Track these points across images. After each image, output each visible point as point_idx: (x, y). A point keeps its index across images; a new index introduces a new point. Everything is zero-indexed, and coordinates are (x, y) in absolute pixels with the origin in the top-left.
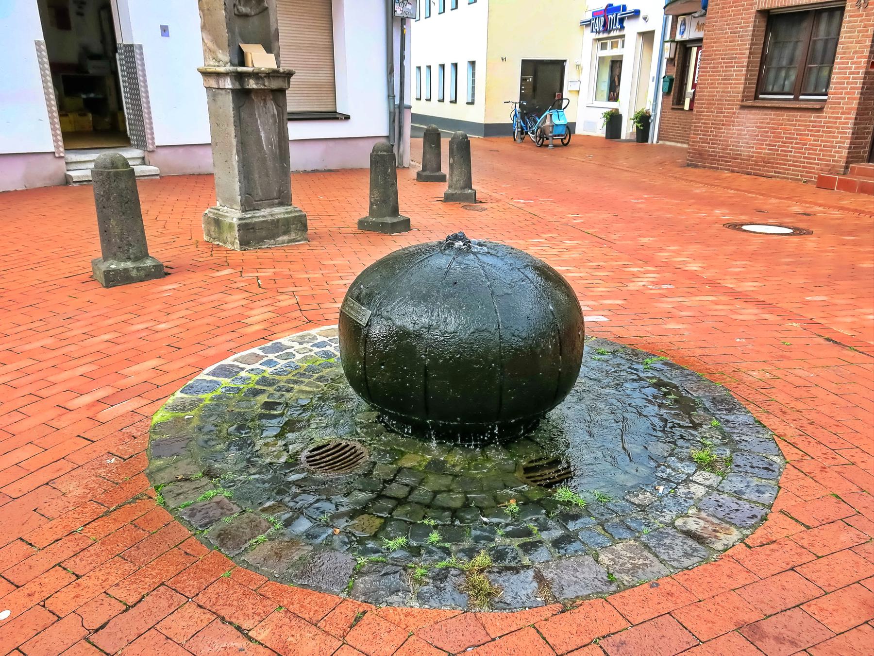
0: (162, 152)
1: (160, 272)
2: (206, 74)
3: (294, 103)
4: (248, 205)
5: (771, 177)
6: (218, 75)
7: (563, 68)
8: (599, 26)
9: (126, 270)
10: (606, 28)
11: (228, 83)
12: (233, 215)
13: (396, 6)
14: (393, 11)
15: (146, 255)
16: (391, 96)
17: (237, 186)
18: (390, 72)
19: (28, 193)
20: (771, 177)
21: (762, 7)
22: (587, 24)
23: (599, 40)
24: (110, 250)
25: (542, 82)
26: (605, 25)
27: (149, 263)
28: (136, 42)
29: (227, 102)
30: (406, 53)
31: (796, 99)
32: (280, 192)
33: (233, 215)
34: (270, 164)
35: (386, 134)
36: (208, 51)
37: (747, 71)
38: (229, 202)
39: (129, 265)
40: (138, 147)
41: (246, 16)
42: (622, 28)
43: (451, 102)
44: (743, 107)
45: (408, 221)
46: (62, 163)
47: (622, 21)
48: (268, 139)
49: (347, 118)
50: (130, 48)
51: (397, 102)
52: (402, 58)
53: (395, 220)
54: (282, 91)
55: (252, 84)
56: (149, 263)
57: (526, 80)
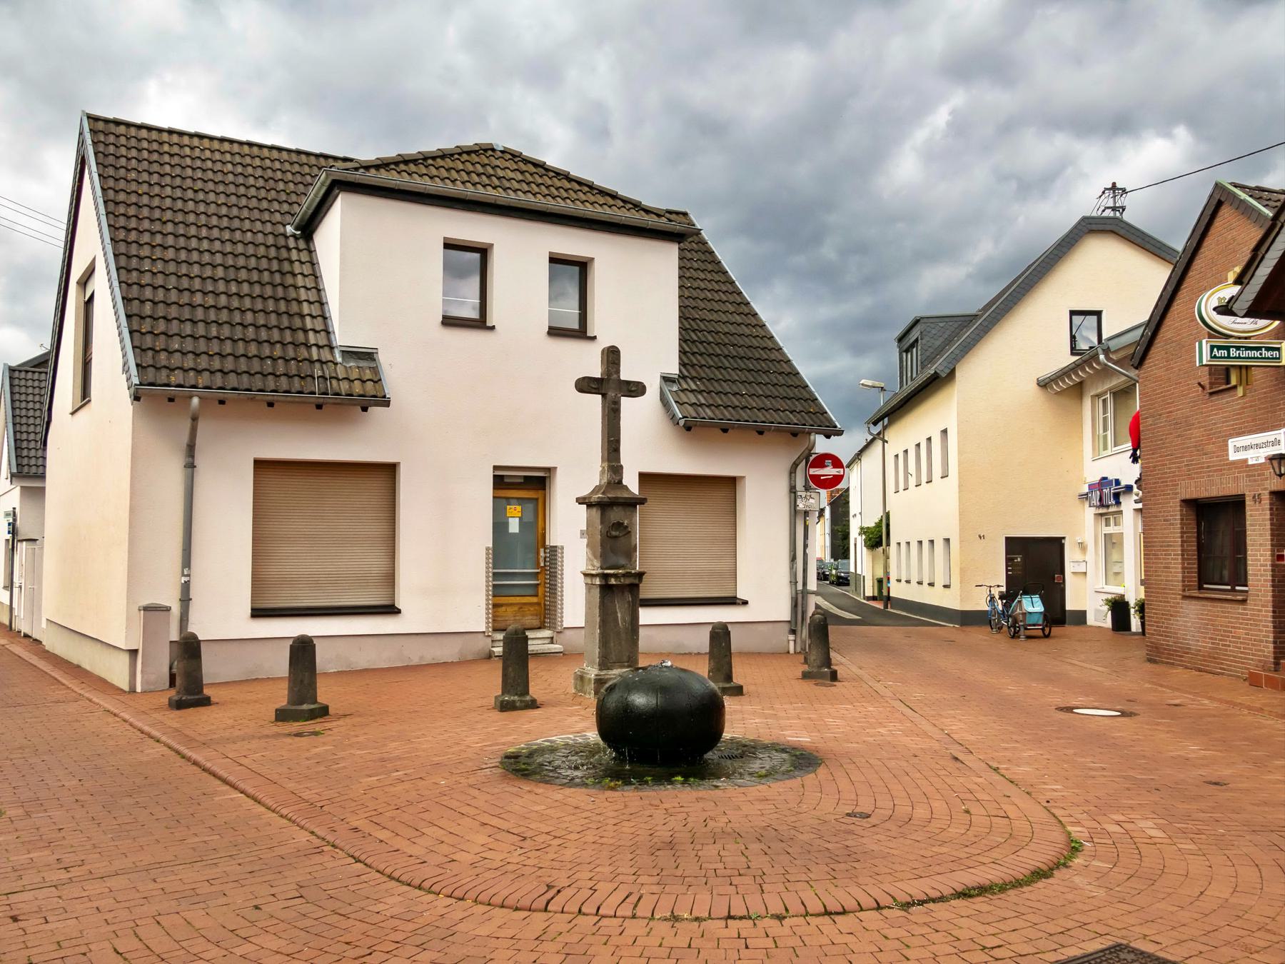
0: (567, 632)
1: (533, 705)
2: (586, 575)
3: (646, 592)
4: (604, 664)
5: (1218, 674)
6: (592, 575)
7: (1062, 547)
8: (1096, 502)
9: (514, 701)
10: (1102, 504)
11: (598, 581)
12: (592, 672)
13: (799, 501)
14: (796, 505)
15: (527, 693)
16: (794, 582)
17: (597, 650)
18: (793, 559)
19: (462, 663)
20: (1218, 674)
21: (1184, 497)
22: (1084, 497)
23: (1101, 515)
24: (506, 688)
25: (1036, 564)
26: (1101, 500)
27: (528, 698)
28: (558, 544)
29: (597, 592)
30: (809, 542)
31: (1233, 590)
32: (629, 658)
33: (592, 672)
34: (623, 636)
35: (788, 619)
36: (589, 559)
37: (1183, 559)
38: (591, 663)
39: (516, 698)
40: (549, 628)
41: (616, 537)
42: (1118, 503)
43: (945, 586)
44: (1185, 597)
45: (741, 687)
46: (489, 640)
47: (1117, 496)
48: (623, 618)
49: (745, 603)
50: (554, 549)
51: (800, 587)
52: (806, 546)
53: (728, 685)
54: (637, 586)
55: (613, 581)
56: (528, 698)
57: (1013, 559)
